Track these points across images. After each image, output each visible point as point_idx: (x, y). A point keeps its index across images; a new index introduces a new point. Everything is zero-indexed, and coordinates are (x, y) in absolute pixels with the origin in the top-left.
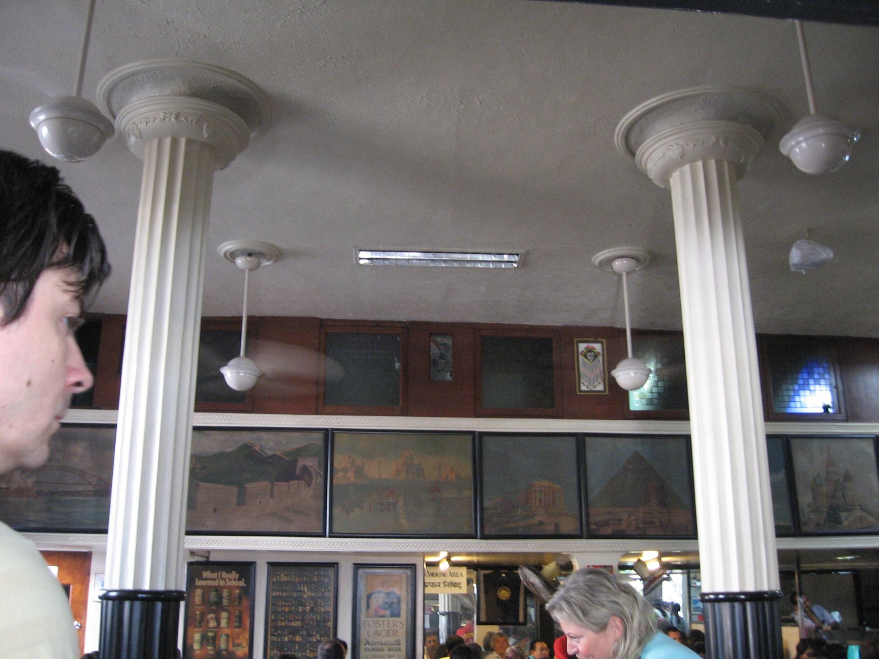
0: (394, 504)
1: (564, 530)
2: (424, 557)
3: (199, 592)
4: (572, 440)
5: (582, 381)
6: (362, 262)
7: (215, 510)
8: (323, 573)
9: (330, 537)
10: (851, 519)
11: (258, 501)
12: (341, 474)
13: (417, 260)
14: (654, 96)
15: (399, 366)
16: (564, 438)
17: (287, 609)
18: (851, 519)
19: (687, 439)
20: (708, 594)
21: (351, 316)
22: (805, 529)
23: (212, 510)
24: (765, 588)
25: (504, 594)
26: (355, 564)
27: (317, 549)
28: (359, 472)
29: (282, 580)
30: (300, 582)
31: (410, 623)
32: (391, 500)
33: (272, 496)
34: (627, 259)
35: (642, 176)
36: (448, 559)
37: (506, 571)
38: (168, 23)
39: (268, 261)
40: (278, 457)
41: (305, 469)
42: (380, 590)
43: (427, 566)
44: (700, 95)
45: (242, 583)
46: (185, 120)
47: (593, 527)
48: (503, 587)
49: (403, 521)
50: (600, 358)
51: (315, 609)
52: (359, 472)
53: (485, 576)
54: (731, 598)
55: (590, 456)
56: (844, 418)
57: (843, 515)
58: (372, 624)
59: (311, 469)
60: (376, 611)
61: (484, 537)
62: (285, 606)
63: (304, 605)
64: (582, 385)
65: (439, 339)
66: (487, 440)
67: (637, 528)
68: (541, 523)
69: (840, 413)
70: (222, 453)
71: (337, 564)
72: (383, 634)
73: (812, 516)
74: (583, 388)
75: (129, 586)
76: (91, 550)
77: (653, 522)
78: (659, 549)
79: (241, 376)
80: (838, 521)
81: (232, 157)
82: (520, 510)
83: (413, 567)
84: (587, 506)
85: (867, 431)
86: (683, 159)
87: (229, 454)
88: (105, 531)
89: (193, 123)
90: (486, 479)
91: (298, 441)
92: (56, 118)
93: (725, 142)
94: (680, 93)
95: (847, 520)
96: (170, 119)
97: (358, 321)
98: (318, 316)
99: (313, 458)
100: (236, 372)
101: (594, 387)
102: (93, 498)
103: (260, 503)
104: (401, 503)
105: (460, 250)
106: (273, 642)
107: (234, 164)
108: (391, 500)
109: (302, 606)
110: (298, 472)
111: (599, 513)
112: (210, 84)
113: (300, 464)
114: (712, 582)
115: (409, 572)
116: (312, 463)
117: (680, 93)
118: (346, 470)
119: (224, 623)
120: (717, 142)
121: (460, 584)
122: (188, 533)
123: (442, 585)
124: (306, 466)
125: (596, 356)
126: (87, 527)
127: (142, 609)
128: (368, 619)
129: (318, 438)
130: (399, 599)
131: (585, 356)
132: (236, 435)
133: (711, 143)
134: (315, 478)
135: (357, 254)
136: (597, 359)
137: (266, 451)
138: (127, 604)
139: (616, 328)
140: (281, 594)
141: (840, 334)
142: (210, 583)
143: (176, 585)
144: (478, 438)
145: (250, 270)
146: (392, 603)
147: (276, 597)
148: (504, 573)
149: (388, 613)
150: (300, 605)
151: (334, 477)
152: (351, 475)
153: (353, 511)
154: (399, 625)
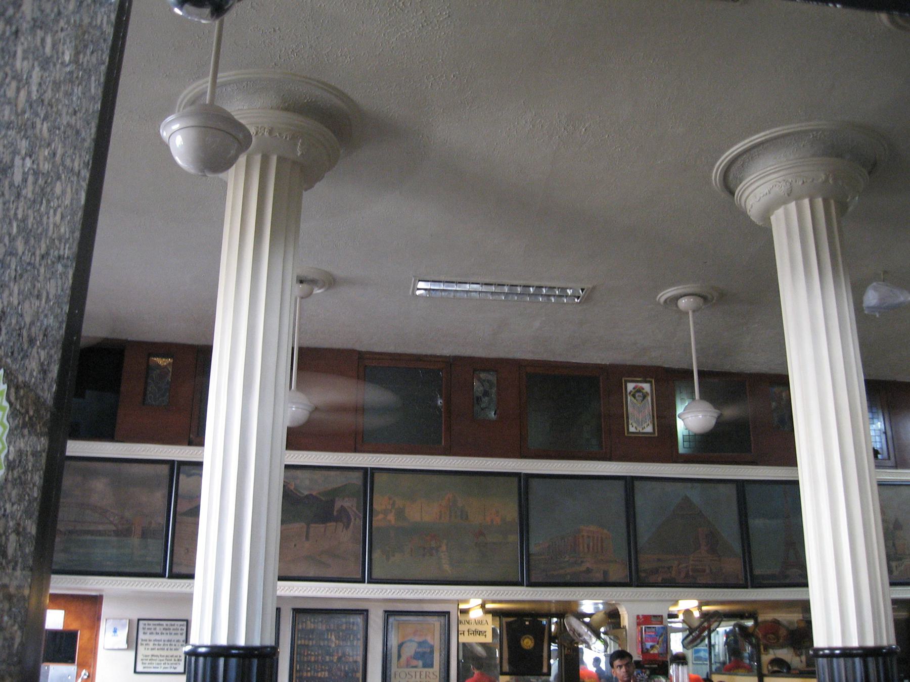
1: (613, 578)
2: (458, 605)
4: (622, 483)
5: (630, 422)
6: (418, 293)
8: (352, 620)
9: (369, 582)
10: (902, 568)
12: (381, 516)
13: (476, 292)
14: (764, 130)
15: (441, 403)
16: (604, 482)
18: (902, 568)
19: (796, 483)
20: (823, 649)
21: (391, 349)
24: (885, 643)
25: (528, 643)
26: (386, 612)
29: (309, 627)
30: (328, 630)
31: (443, 675)
32: (433, 544)
34: (694, 297)
35: (743, 214)
36: (483, 606)
37: (529, 619)
38: (275, 31)
39: (320, 289)
41: (343, 509)
42: (413, 639)
43: (460, 613)
44: (812, 131)
46: (279, 135)
47: (643, 575)
49: (447, 567)
50: (649, 398)
51: (343, 659)
52: (400, 514)
53: (508, 624)
54: (847, 653)
55: (639, 500)
56: (893, 464)
58: (403, 675)
59: (349, 510)
60: (408, 660)
61: (531, 584)
63: (331, 655)
64: (630, 426)
65: (483, 375)
66: (534, 483)
67: (687, 575)
68: (588, 571)
69: (889, 458)
71: (367, 611)
74: (632, 429)
75: (223, 641)
76: (101, 593)
78: (698, 598)
79: (293, 411)
81: (319, 178)
82: (567, 557)
83: (447, 614)
84: (636, 552)
85: (902, 478)
86: (791, 195)
88: (191, 576)
89: (288, 139)
90: (532, 522)
91: (338, 480)
92: (193, 127)
93: (835, 179)
94: (791, 128)
96: (263, 134)
97: (400, 355)
98: (358, 348)
100: (710, 416)
101: (643, 429)
102: (114, 539)
103: (295, 545)
104: (444, 548)
105: (459, 279)
107: (318, 186)
108: (433, 544)
109: (330, 655)
110: (335, 513)
111: (647, 561)
112: (306, 98)
113: (338, 504)
114: (829, 635)
115: (442, 619)
116: (349, 504)
117: (791, 128)
118: (386, 512)
120: (826, 180)
121: (485, 632)
122: (281, 578)
123: (466, 633)
125: (644, 396)
126: (107, 570)
127: (238, 666)
128: (400, 670)
129: (357, 479)
130: (432, 647)
131: (634, 396)
133: (820, 180)
134: (353, 520)
135: (415, 285)
136: (645, 400)
137: (302, 491)
138: (222, 661)
139: (665, 367)
140: (307, 643)
141: (888, 378)
143: (262, 639)
144: (524, 480)
145: (302, 298)
146: (424, 653)
147: (301, 645)
148: (527, 621)
149: (420, 663)
150: (327, 655)
151: (374, 519)
152: (391, 517)
154: (431, 675)
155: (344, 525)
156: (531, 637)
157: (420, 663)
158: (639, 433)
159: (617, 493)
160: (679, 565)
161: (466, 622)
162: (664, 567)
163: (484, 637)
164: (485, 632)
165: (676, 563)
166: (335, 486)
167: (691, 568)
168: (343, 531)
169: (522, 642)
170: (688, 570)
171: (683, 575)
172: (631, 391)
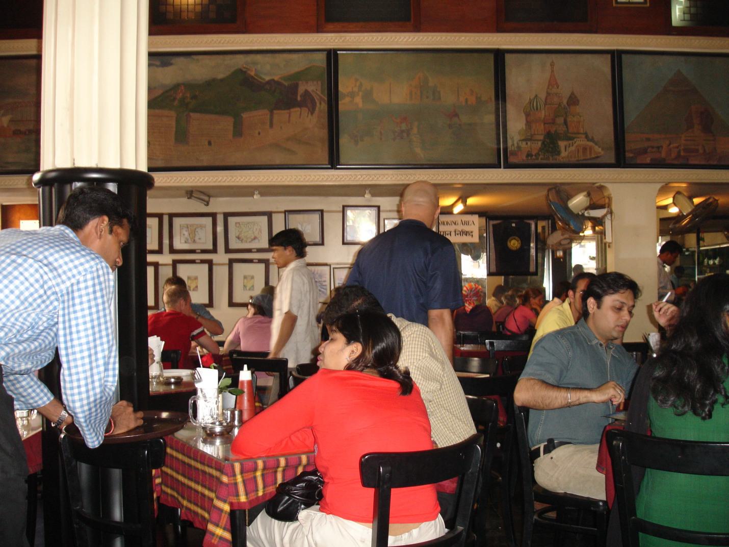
0: (408, 132)
7: (210, 143)
11: (257, 132)
12: (347, 100)
18: (573, 148)
23: (207, 143)
27: (172, 184)
28: (368, 96)
33: (271, 125)
40: (278, 83)
48: (511, 238)
49: (418, 150)
52: (368, 96)
57: (562, 144)
59: (314, 95)
67: (678, 156)
70: (214, 80)
73: (523, 145)
77: (697, 151)
87: (222, 80)
91: (298, 64)
95: (566, 150)
99: (315, 83)
103: (259, 134)
104: (415, 130)
108: (404, 126)
110: (299, 98)
111: (633, 142)
113: (301, 89)
118: (352, 95)
124: (308, 92)
129: (321, 59)
132: (228, 59)
134: (318, 104)
137: (263, 77)
148: (514, 223)
152: (358, 100)
153: (362, 140)
155: (309, 110)
156: (517, 238)
159: (604, 65)
160: (670, 144)
161: (450, 223)
162: (653, 147)
163: (470, 237)
164: (472, 232)
165: (668, 142)
166: (296, 69)
167: (682, 147)
168: (308, 116)
169: (508, 243)
170: (680, 150)
171: (673, 155)
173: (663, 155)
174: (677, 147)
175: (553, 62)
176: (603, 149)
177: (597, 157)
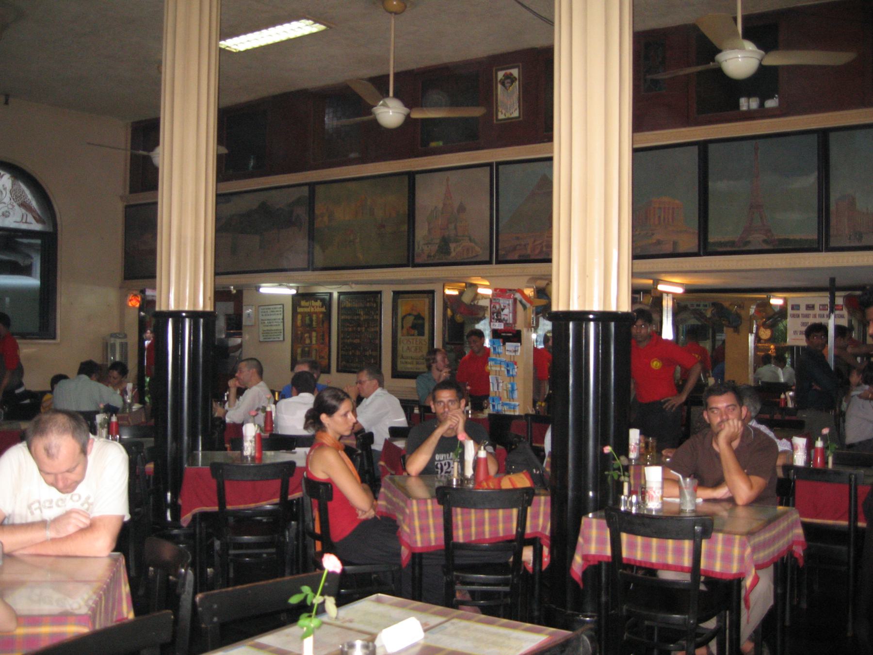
1: (681, 249)
3: (299, 317)
5: (500, 109)
9: (497, 263)
17: (350, 329)
18: (459, 249)
22: (418, 260)
45: (323, 310)
57: (452, 246)
62: (350, 327)
66: (711, 147)
68: (659, 242)
72: (413, 349)
73: (425, 248)
74: (516, 114)
80: (448, 252)
91: (296, 193)
101: (511, 114)
106: (342, 355)
116: (301, 212)
119: (314, 339)
128: (403, 338)
142: (306, 310)
152: (326, 219)
157: (416, 332)
158: (509, 119)
160: (535, 241)
171: (537, 251)
172: (501, 80)
173: (529, 252)
174: (541, 244)
175: (448, 177)
176: (481, 248)
177: (477, 256)
